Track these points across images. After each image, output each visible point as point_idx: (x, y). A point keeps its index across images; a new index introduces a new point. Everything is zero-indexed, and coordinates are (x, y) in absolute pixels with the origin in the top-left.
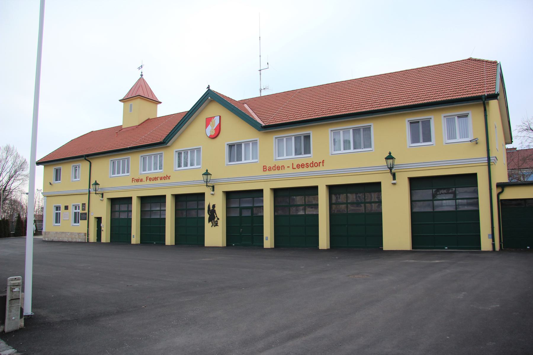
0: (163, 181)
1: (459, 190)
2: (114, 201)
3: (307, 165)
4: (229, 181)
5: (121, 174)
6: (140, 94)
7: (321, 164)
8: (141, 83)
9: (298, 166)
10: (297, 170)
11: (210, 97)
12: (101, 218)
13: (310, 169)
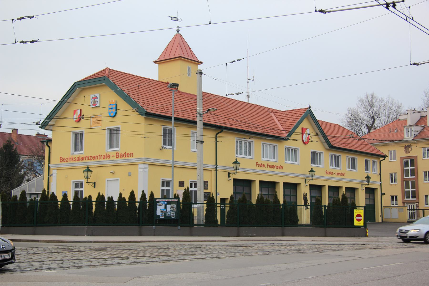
0: (278, 170)
5: (247, 156)
8: (179, 41)
11: (308, 114)
12: (179, 186)
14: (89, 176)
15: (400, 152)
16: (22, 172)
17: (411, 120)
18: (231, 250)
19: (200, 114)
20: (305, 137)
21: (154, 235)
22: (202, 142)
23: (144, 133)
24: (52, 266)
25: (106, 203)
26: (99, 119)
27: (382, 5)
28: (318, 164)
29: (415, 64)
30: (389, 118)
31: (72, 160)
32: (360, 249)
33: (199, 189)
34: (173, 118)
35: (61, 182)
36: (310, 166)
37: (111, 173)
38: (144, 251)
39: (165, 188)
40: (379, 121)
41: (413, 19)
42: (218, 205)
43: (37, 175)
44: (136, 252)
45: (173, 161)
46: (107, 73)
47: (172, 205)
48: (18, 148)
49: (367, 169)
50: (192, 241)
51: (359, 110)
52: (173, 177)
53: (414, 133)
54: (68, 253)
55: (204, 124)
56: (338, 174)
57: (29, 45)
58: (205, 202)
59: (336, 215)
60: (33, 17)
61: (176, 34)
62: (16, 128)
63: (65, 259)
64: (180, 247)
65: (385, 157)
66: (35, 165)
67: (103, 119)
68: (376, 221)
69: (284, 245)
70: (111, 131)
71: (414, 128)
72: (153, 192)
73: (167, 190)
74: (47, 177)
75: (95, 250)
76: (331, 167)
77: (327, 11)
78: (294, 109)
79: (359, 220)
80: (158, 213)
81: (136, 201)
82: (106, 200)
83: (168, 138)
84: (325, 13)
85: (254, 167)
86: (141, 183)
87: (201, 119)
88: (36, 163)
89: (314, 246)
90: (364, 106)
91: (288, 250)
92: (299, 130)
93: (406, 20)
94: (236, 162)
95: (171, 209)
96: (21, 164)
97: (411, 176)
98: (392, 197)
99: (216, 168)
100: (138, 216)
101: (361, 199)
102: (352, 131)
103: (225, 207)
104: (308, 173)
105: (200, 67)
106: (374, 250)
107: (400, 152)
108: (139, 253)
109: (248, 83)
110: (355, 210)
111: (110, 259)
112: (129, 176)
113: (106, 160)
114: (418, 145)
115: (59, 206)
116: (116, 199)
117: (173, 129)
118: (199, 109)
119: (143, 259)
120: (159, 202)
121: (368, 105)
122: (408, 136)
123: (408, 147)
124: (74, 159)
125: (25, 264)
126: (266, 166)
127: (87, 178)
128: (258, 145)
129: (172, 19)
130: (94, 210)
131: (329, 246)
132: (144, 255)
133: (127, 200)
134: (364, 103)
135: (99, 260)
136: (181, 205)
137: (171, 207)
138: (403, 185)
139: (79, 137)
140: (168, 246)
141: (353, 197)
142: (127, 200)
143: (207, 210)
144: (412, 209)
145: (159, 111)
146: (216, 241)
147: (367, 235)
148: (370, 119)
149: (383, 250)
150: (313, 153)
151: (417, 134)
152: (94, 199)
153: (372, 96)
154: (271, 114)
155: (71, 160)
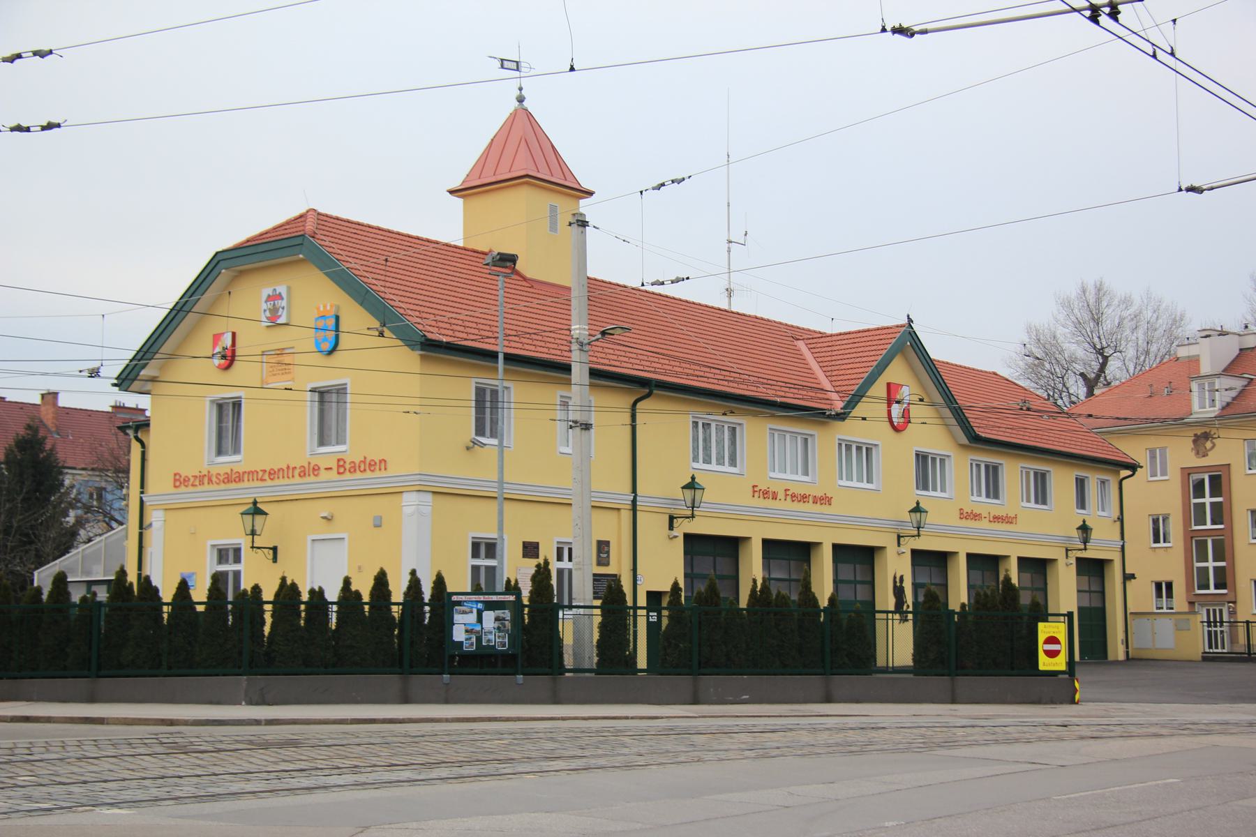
0: (818, 508)
2: (698, 546)
8: (522, 128)
11: (907, 342)
12: (524, 556)
14: (258, 528)
15: (1180, 453)
16: (71, 519)
17: (1211, 357)
18: (669, 744)
19: (581, 344)
20: (896, 410)
21: (447, 701)
22: (587, 427)
23: (417, 401)
24: (127, 795)
25: (303, 607)
26: (287, 359)
27: (1078, 11)
28: (935, 489)
29: (1191, 189)
30: (1147, 353)
31: (210, 481)
32: (1049, 740)
33: (578, 563)
34: (501, 356)
35: (172, 545)
36: (913, 495)
37: (324, 518)
38: (408, 750)
39: (483, 562)
40: (1119, 364)
41: (1172, 54)
42: (640, 612)
43: (114, 524)
44: (385, 752)
45: (501, 482)
46: (310, 226)
47: (499, 613)
48: (59, 448)
49: (1081, 503)
50: (558, 719)
51: (1060, 331)
52: (501, 529)
53: (1222, 398)
54: (183, 756)
55: (594, 373)
56: (997, 519)
57: (37, 137)
58: (598, 603)
59: (984, 638)
60: (51, 52)
61: (516, 110)
62: (53, 388)
63: (170, 772)
64: (518, 736)
65: (1133, 467)
66: (109, 497)
67: (298, 359)
68: (1111, 657)
69: (828, 729)
70: (322, 394)
71: (1221, 383)
72: (444, 574)
73: (487, 567)
74: (137, 531)
75: (266, 745)
76: (975, 498)
77: (916, 29)
78: (866, 327)
79: (1052, 654)
80: (459, 634)
81: (165, 600)
82: (305, 597)
83: (487, 412)
84: (912, 35)
85: (954, 520)
86: (411, 546)
87: (585, 358)
88: (112, 492)
89: (914, 731)
90: (1073, 318)
91: (837, 744)
92: (879, 389)
93: (1154, 56)
94: (692, 485)
95: (496, 625)
96: (67, 493)
97: (1213, 523)
98: (1158, 586)
99: (634, 502)
100: (400, 645)
101: (1066, 592)
102: (1040, 392)
103: (659, 617)
104: (907, 517)
105: (585, 206)
106: (1092, 742)
107: (1180, 453)
108: (395, 755)
109: (729, 251)
110: (1041, 625)
111: (304, 774)
112: (376, 526)
113: (307, 479)
115: (165, 616)
116: (332, 594)
117: (500, 389)
118: (579, 329)
119: (402, 773)
120: (459, 603)
121: (1087, 317)
122: (1202, 407)
123: (1202, 439)
124: (214, 479)
125: (50, 789)
126: (781, 495)
127: (253, 533)
128: (755, 432)
129: (502, 67)
130: (267, 629)
131: (960, 732)
132: (408, 760)
133: (366, 598)
134: (1076, 311)
135: (272, 775)
136: (526, 610)
137: (497, 619)
138: (1188, 551)
139: (228, 414)
140: (485, 732)
141: (1041, 586)
142: (366, 598)
143: (602, 627)
144: (1215, 622)
145: (464, 336)
146: (627, 718)
147: (1077, 697)
148: (1093, 356)
149: (1119, 743)
150: (922, 458)
151: (1229, 400)
152: (268, 594)
153: (1099, 289)
154: (796, 343)
155: (206, 480)
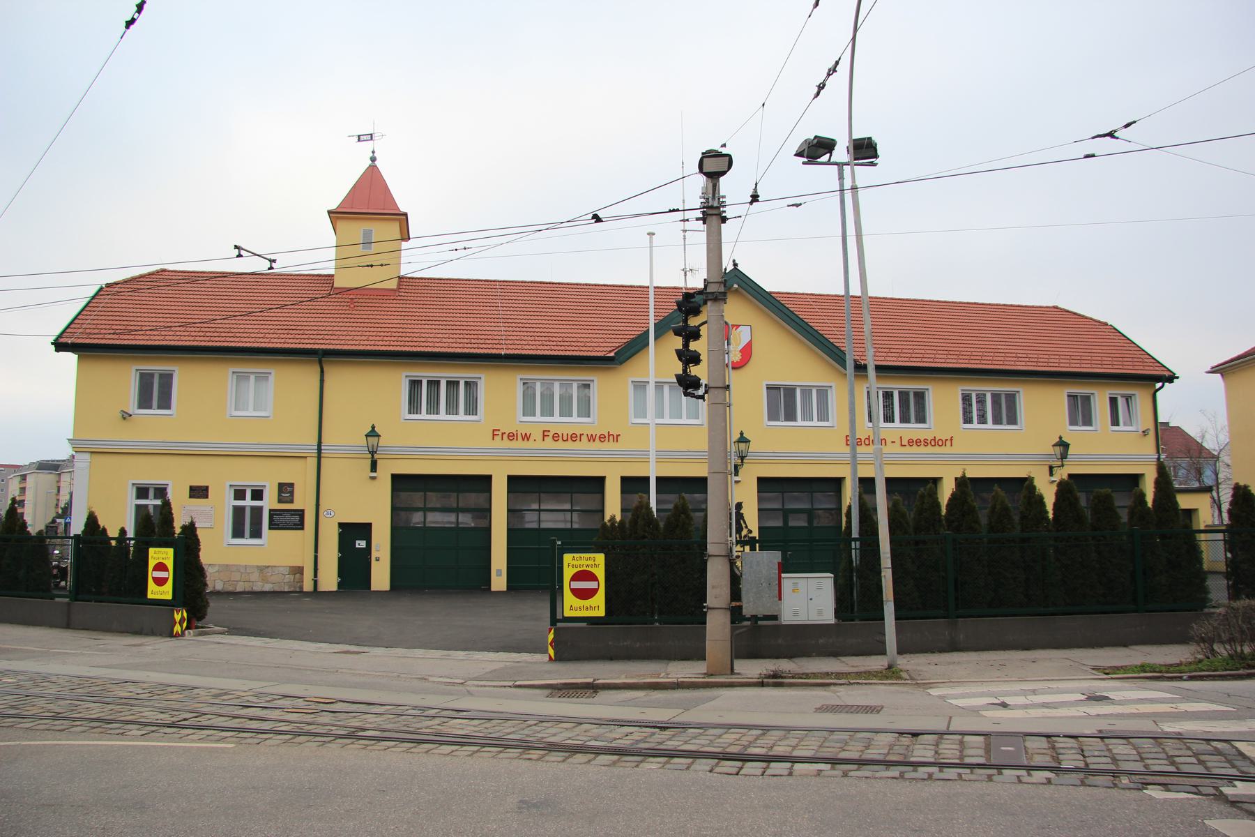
1: (818, 495)
3: (926, 443)
4: (775, 457)
6: (369, 207)
7: (948, 443)
8: (372, 181)
9: (910, 442)
10: (908, 450)
12: (207, 497)
13: (929, 449)
55: (879, 368)
85: (486, 442)
114: (261, 266)
